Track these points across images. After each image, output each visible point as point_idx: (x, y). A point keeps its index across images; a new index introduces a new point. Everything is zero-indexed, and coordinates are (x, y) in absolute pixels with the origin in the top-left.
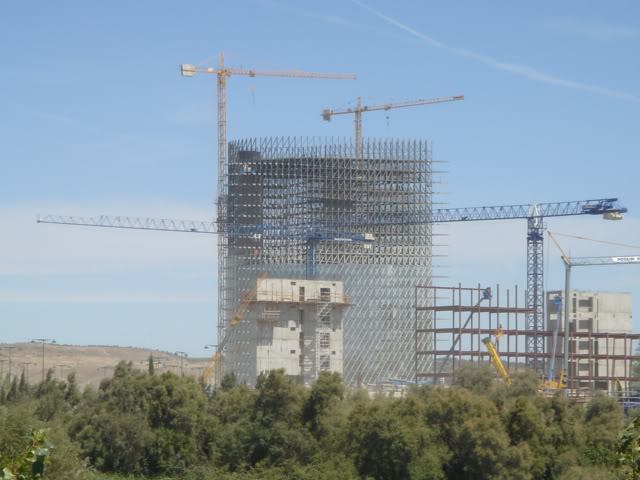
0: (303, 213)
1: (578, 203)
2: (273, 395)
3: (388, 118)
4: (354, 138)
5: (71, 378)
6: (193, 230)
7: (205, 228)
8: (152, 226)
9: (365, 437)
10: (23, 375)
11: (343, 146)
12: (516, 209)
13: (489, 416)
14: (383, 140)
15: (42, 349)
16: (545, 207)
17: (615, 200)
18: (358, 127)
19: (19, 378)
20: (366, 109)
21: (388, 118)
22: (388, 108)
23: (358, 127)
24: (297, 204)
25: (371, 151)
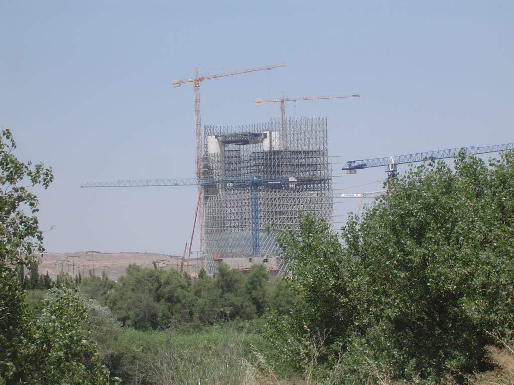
0: (251, 173)
1: (439, 152)
2: (227, 281)
3: (295, 106)
4: (281, 119)
5: (104, 274)
6: (176, 185)
7: (190, 182)
8: (150, 184)
9: (407, 271)
10: (79, 274)
11: (274, 123)
12: (376, 161)
13: (140, 365)
14: (300, 118)
15: (93, 255)
16: (398, 158)
17: (46, 188)
18: (283, 111)
19: (78, 274)
20: (287, 100)
21: (295, 106)
22: (295, 101)
23: (283, 111)
24: (247, 167)
25: (256, 129)
